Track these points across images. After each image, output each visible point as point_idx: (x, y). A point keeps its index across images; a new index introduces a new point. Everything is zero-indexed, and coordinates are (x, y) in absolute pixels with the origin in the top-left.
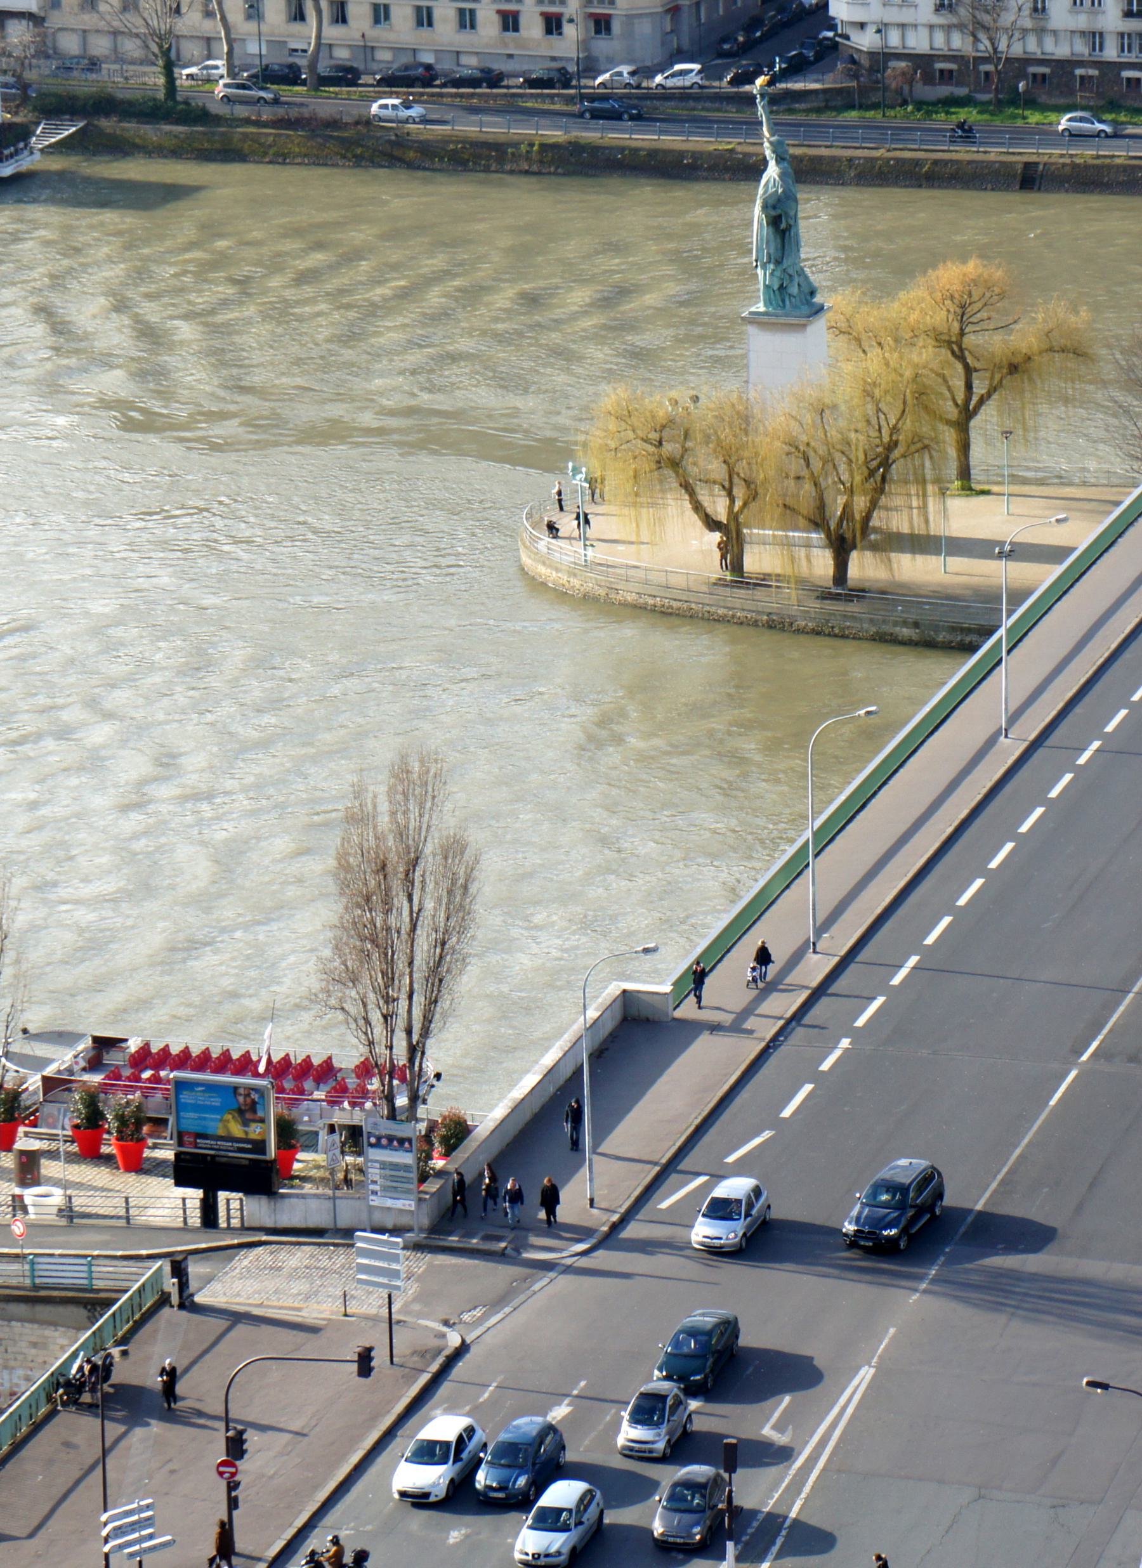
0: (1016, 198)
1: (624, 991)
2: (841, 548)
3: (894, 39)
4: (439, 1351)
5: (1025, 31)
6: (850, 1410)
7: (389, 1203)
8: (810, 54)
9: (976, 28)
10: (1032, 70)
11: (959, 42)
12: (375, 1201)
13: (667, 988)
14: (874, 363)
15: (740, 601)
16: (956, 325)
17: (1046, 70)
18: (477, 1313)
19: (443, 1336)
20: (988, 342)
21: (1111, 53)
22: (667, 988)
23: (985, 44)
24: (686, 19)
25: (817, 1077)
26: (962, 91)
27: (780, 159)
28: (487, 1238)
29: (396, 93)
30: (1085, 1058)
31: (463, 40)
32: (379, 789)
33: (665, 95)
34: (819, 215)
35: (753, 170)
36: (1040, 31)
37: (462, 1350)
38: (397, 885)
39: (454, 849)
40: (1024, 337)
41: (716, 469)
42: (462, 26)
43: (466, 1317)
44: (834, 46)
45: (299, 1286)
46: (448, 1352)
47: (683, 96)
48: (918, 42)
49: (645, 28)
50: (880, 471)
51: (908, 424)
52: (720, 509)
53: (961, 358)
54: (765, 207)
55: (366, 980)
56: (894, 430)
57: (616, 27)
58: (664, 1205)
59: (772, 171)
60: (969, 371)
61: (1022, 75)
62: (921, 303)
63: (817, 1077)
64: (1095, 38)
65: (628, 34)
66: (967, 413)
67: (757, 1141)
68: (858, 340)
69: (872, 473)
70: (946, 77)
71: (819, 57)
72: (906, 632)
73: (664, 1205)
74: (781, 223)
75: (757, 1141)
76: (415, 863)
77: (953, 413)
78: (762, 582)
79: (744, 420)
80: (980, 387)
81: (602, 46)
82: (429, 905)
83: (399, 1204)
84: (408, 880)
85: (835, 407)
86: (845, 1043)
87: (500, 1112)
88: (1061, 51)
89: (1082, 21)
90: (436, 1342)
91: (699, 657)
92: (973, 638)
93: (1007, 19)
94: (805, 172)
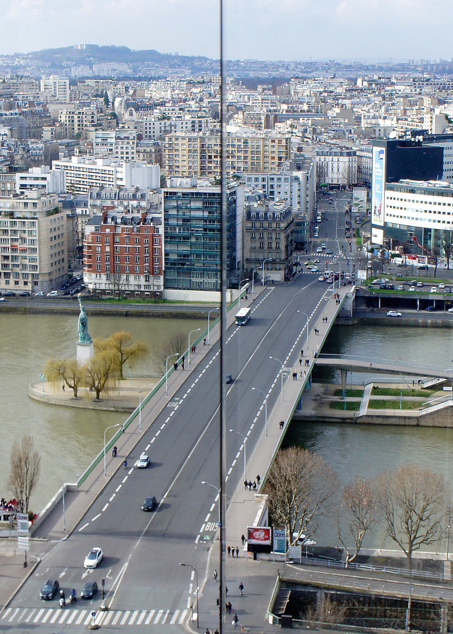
0: (125, 318)
1: (67, 486)
2: (98, 391)
3: (98, 286)
4: (36, 562)
5: (125, 285)
6: (124, 572)
7: (22, 531)
8: (79, 289)
9: (115, 284)
10: (126, 292)
11: (112, 287)
12: (20, 531)
13: (76, 484)
14: (103, 353)
15: (77, 404)
16: (119, 345)
17: (129, 292)
18: (43, 554)
19: (36, 559)
20: (126, 348)
21: (142, 289)
22: (76, 484)
23: (116, 288)
24: (54, 282)
25: (109, 502)
26: (112, 297)
27: (84, 311)
28: (43, 538)
29: (305, 332)
30: (165, 497)
31: (7, 287)
32: (20, 443)
33: (50, 298)
34: (91, 322)
35: (77, 313)
36: (128, 285)
37: (40, 562)
38: (23, 463)
39: (36, 455)
40: (133, 347)
41: (71, 375)
42: (6, 284)
43: (41, 555)
44: (85, 287)
45: (4, 549)
46: (38, 562)
47: (54, 298)
48: (103, 287)
49: (45, 284)
50: (106, 375)
51: (112, 366)
52: (72, 383)
53: (120, 352)
54: (81, 320)
55: (16, 484)
56: (109, 366)
57: (39, 283)
58: (80, 530)
59: (82, 314)
60: (122, 354)
61: (124, 293)
62: (111, 340)
63: (109, 502)
64: (139, 286)
65: (42, 285)
66: (122, 363)
67: (98, 516)
68: (99, 348)
69: (105, 375)
70: (109, 293)
71: (81, 290)
72: (112, 409)
73: (80, 530)
74: (84, 324)
75: (98, 516)
76: (27, 459)
77: (119, 363)
78: (81, 398)
79: (75, 364)
80: (124, 358)
81: (36, 288)
82: (30, 468)
83: (25, 531)
84: (26, 463)
85: (96, 362)
86: (114, 495)
87: (44, 511)
88: (132, 289)
89: (136, 283)
90: (35, 560)
91: (67, 414)
92: (131, 410)
93: (121, 282)
94: (87, 313)
